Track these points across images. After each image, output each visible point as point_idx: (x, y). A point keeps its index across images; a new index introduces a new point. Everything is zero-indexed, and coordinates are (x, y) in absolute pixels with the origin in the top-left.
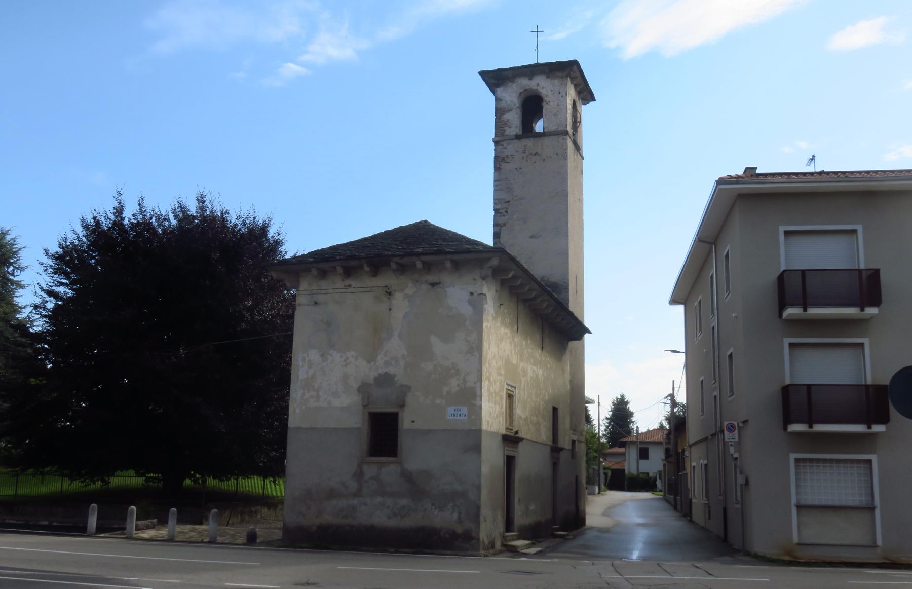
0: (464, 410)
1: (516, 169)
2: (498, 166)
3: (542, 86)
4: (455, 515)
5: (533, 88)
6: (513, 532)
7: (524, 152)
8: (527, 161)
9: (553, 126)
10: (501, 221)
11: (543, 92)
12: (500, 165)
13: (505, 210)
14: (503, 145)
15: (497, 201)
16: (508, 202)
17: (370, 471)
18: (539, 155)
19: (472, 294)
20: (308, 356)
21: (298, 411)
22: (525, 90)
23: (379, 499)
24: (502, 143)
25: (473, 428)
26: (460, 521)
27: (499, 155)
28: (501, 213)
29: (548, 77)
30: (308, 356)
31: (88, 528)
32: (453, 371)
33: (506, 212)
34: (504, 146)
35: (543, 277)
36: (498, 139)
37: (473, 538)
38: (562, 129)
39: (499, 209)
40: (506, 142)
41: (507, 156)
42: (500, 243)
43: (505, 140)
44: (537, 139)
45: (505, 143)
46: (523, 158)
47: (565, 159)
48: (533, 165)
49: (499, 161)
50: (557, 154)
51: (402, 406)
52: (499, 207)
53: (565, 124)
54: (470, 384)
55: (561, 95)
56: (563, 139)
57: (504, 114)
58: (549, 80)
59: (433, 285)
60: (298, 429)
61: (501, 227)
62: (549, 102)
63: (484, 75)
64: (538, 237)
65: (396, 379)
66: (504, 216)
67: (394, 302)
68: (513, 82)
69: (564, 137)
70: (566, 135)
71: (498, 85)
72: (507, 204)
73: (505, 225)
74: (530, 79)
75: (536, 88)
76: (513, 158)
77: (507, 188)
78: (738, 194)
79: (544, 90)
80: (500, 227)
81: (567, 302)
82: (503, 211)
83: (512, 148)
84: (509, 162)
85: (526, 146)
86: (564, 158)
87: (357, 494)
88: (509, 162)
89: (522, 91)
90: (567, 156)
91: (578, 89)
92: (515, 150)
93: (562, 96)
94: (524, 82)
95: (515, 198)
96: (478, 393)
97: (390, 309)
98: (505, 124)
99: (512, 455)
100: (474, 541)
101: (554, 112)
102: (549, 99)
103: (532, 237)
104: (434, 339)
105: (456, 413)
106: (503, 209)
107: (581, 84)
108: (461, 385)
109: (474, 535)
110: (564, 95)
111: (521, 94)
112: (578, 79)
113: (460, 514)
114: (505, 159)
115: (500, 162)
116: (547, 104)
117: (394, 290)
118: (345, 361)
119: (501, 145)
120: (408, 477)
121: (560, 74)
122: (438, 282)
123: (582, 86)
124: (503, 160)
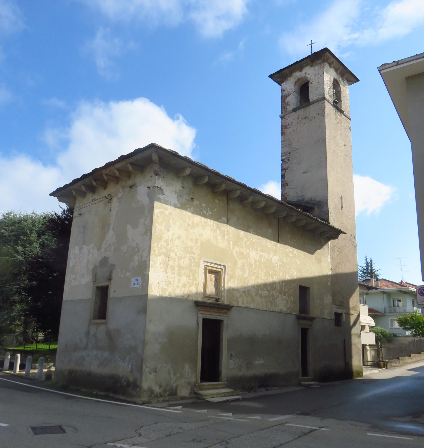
0: (140, 279)
1: (294, 131)
2: (283, 132)
3: (308, 74)
4: (130, 366)
5: (303, 76)
6: (221, 382)
7: (298, 119)
8: (300, 124)
9: (315, 97)
10: (286, 166)
11: (309, 77)
12: (284, 131)
13: (288, 159)
14: (286, 118)
15: (283, 154)
16: (289, 153)
17: (93, 330)
18: (307, 118)
19: (149, 188)
20: (74, 251)
21: (67, 290)
22: (298, 80)
23: (95, 352)
24: (285, 117)
25: (144, 294)
26: (132, 372)
27: (284, 125)
28: (286, 161)
29: (311, 66)
30: (74, 251)
31: (4, 367)
32: (136, 250)
33: (289, 160)
34: (287, 118)
35: (312, 199)
36: (282, 115)
37: (138, 387)
38: (321, 97)
39: (284, 159)
40: (287, 115)
41: (288, 124)
42: (285, 181)
43: (287, 114)
44: (306, 108)
45: (287, 117)
46: (298, 122)
47: (323, 116)
48: (304, 125)
49: (284, 129)
50: (318, 114)
51: (110, 279)
52: (284, 158)
53: (323, 93)
54: (144, 259)
55: (320, 75)
56: (322, 103)
57: (286, 98)
58: (312, 68)
59: (131, 187)
60: (67, 301)
61: (286, 170)
62: (313, 82)
63: (271, 76)
64: (308, 172)
65: (109, 260)
66: (287, 163)
67: (112, 205)
68: (291, 76)
69: (323, 102)
70: (324, 100)
71: (282, 82)
72: (289, 155)
73: (288, 168)
74: (301, 71)
75: (304, 76)
76: (292, 124)
77: (289, 144)
78: (406, 78)
79: (310, 75)
80: (284, 171)
81: (327, 213)
82: (286, 160)
83: (292, 118)
84: (290, 128)
85: (299, 115)
86: (323, 115)
87: (85, 348)
88: (290, 128)
89: (296, 80)
90: (325, 114)
91: (338, 72)
92: (293, 119)
93: (321, 76)
94: (297, 74)
95: (293, 150)
96: (148, 266)
97: (111, 210)
98: (286, 105)
99: (221, 319)
100: (138, 389)
101: (315, 88)
102: (313, 80)
103: (304, 173)
104: (129, 227)
105: (135, 282)
106: (287, 158)
107: (340, 68)
108: (139, 260)
109: (138, 384)
110: (322, 74)
111: (296, 83)
112: (335, 63)
113: (132, 365)
114: (287, 126)
115: (284, 129)
116: (312, 84)
117: (113, 196)
118: (89, 251)
119: (285, 118)
120: (109, 335)
121: (318, 62)
122: (133, 184)
123: (341, 69)
124: (286, 127)
